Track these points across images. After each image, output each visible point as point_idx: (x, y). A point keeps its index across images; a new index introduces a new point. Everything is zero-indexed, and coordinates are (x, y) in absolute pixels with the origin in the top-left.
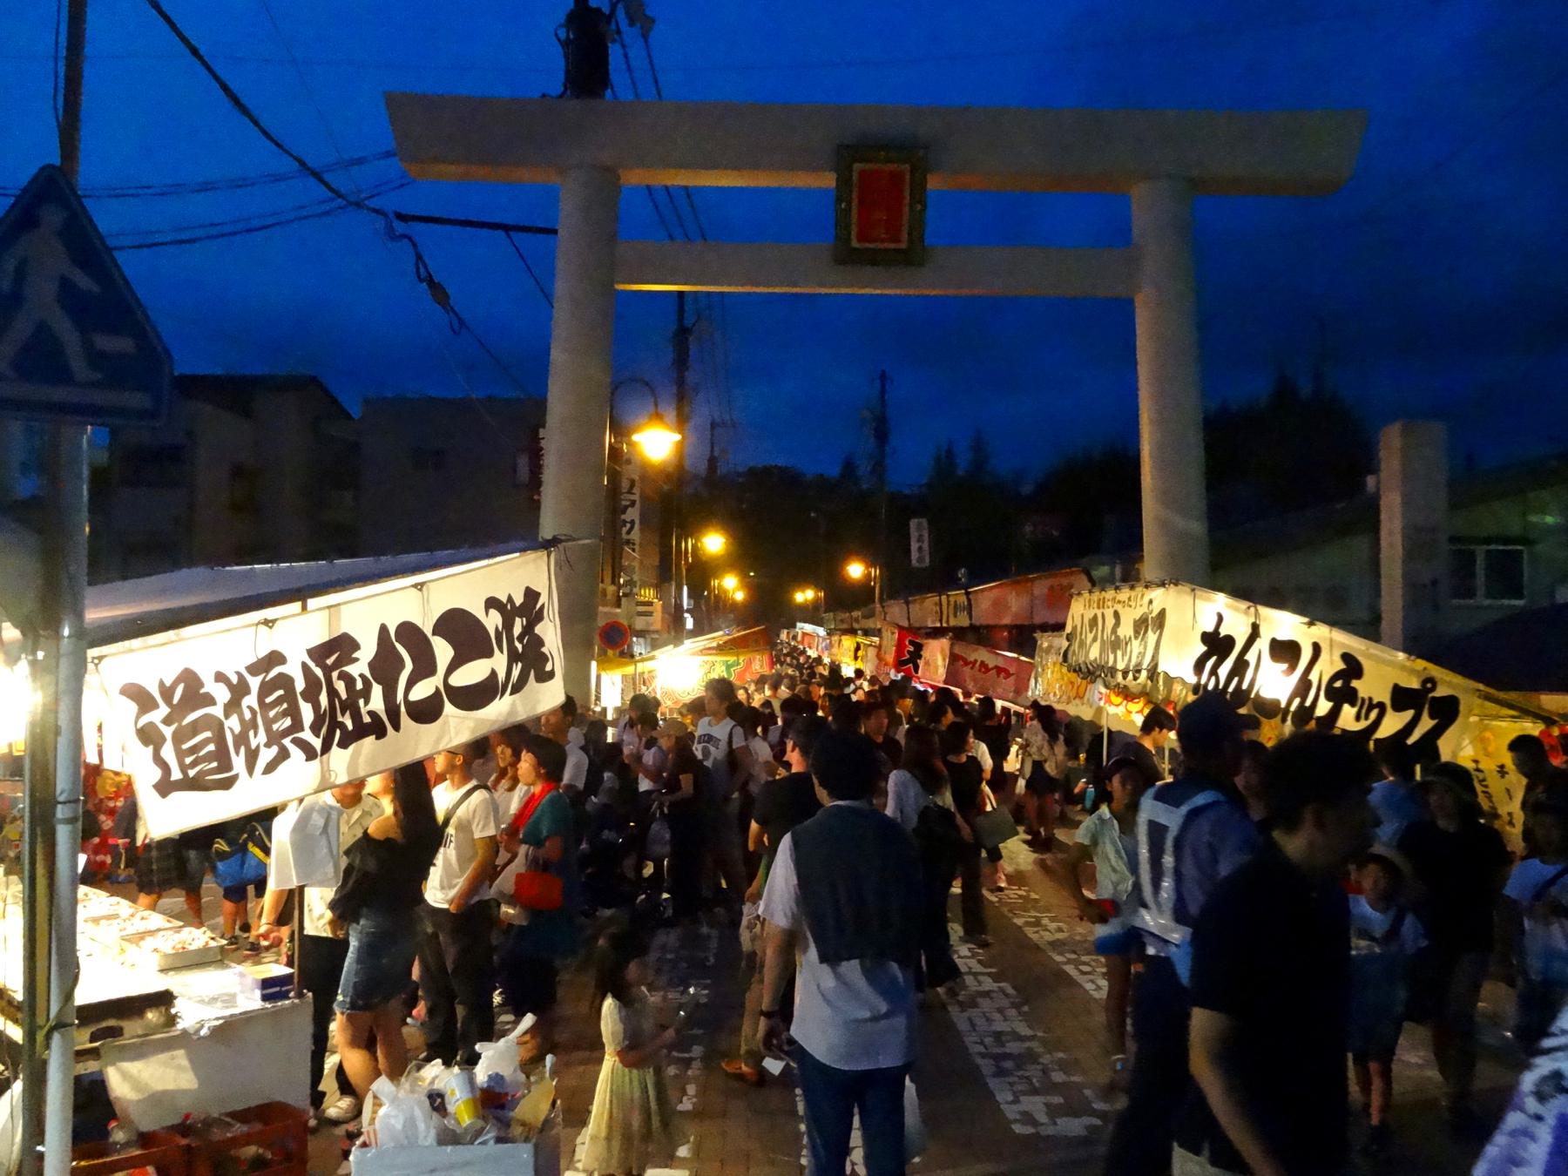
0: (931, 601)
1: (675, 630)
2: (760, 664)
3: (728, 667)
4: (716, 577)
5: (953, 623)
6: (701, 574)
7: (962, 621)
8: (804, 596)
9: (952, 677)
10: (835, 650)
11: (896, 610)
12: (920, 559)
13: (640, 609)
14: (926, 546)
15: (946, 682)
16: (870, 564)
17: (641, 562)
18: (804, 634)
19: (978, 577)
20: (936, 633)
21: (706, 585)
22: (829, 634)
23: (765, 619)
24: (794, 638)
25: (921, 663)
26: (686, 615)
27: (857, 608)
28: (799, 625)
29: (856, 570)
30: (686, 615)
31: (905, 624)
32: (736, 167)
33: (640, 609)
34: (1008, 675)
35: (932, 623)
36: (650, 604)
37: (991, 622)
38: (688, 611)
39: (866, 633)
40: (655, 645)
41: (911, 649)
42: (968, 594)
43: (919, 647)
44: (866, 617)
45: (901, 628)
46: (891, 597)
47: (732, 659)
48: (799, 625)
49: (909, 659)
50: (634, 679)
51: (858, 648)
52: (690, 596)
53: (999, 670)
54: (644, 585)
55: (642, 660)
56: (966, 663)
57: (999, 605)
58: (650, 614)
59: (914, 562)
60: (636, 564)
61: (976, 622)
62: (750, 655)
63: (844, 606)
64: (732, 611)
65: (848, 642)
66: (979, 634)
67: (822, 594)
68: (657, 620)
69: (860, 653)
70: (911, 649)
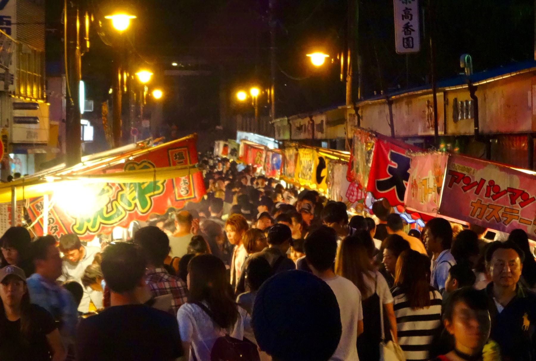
0: (423, 100)
1: (67, 145)
2: (185, 188)
3: (142, 193)
4: (127, 68)
5: (452, 129)
6: (104, 63)
7: (466, 127)
8: (248, 94)
9: (450, 205)
10: (290, 169)
11: (376, 115)
12: (408, 42)
13: (19, 113)
14: (415, 24)
15: (442, 211)
16: (264, 86)
17: (20, 49)
18: (248, 147)
19: (488, 66)
20: (429, 144)
21: (113, 81)
22: (283, 146)
23: (192, 127)
24: (234, 152)
25: (408, 185)
26: (83, 122)
27: (321, 108)
28: (241, 135)
29: (318, 58)
30: (83, 122)
31: (386, 131)
32: (183, 137)
33: (19, 113)
34: (526, 200)
35: (422, 129)
36: (33, 106)
37: (503, 129)
38: (87, 116)
39: (334, 145)
40: (41, 164)
41: (395, 165)
42: (473, 90)
43: (405, 165)
44: (331, 123)
45: (379, 138)
46: (367, 95)
47: (147, 180)
48: (241, 135)
49: (391, 180)
50: (11, 209)
51: (321, 166)
52: (88, 96)
53: (514, 194)
54: (25, 80)
55: (24, 184)
56: (469, 184)
57: (516, 106)
58: (34, 120)
59: (399, 47)
60: (12, 50)
61: (485, 127)
62: (173, 176)
63: (303, 106)
64: (147, 116)
65: (308, 158)
66: (485, 145)
67: (271, 92)
68: (43, 129)
69: (324, 173)
70: (395, 165)
